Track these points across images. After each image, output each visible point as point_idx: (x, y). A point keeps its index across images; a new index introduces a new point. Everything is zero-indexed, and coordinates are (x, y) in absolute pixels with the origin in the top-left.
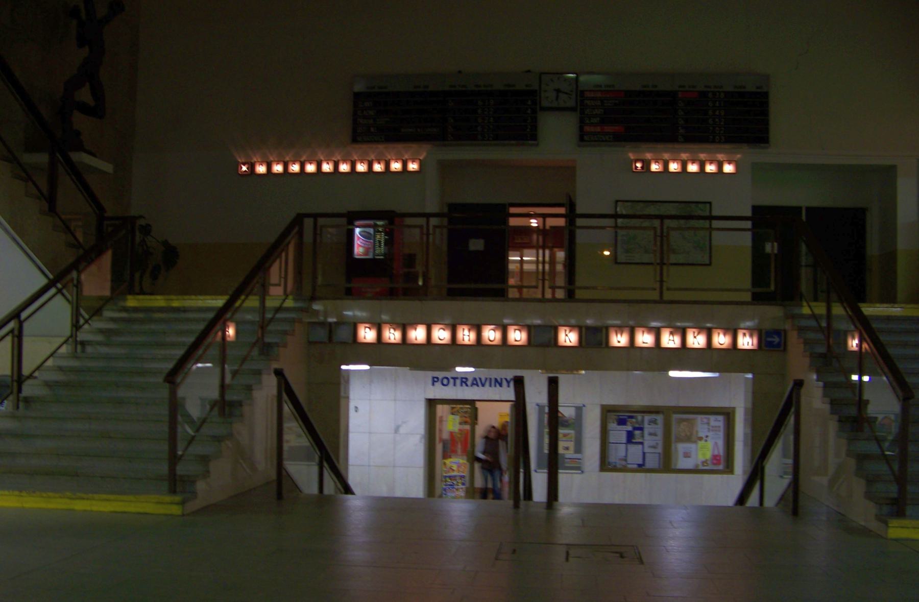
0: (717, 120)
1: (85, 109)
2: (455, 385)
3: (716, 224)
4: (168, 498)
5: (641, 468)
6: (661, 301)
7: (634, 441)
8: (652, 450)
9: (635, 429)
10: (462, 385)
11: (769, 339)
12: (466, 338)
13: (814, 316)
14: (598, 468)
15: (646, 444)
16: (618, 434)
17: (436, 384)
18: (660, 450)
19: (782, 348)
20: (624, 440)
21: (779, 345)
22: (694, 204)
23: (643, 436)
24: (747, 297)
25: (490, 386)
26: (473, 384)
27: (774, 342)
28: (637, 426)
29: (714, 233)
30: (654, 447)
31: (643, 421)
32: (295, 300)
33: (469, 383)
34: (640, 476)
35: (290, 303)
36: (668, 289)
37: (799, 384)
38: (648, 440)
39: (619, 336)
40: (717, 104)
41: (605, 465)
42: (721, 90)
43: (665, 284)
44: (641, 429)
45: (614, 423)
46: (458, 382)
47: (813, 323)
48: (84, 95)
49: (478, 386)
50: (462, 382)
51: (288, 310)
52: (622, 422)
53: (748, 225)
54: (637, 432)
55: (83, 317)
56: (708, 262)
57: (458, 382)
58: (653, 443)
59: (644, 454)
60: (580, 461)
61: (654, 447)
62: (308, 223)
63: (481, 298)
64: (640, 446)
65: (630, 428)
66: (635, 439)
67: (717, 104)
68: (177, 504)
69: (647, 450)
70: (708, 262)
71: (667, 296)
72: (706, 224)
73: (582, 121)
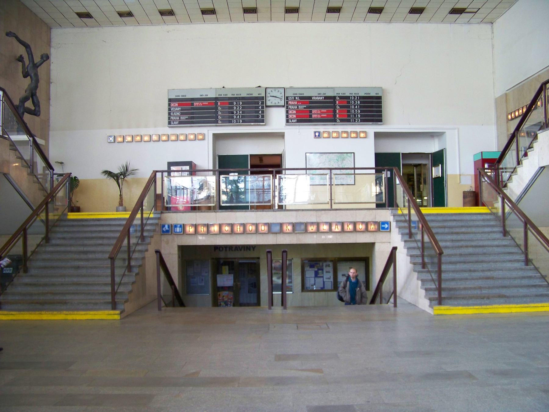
0: (356, 111)
1: (30, 112)
2: (226, 250)
3: (357, 171)
4: (112, 312)
5: (322, 290)
6: (331, 209)
7: (318, 276)
8: (328, 280)
9: (319, 269)
10: (229, 250)
11: (383, 226)
12: (238, 230)
13: (403, 215)
14: (301, 291)
15: (325, 277)
16: (310, 273)
17: (216, 250)
18: (332, 280)
19: (389, 230)
20: (313, 275)
21: (387, 228)
22: (346, 154)
23: (323, 273)
24: (374, 206)
25: (244, 250)
26: (235, 250)
27: (385, 227)
28: (320, 268)
29: (356, 176)
30: (329, 279)
31: (323, 266)
32: (154, 213)
33: (233, 249)
34: (322, 293)
35: (152, 216)
36: (334, 203)
37: (395, 249)
38: (326, 275)
39: (312, 227)
40: (356, 107)
41: (304, 288)
42: (358, 95)
43: (333, 201)
44: (322, 270)
45: (308, 267)
46: (228, 249)
47: (403, 218)
48: (29, 104)
49: (238, 250)
50: (230, 249)
51: (152, 219)
52: (312, 266)
53: (373, 171)
54: (320, 271)
55: (346, 297)
56: (354, 184)
57: (228, 249)
58: (329, 277)
59: (324, 282)
60: (292, 287)
61: (329, 279)
62: (159, 175)
63: (244, 210)
64: (322, 279)
65: (316, 269)
66: (319, 275)
67: (356, 107)
68: (118, 314)
69: (325, 280)
70: (354, 184)
71: (334, 207)
72: (352, 171)
73: (287, 112)
